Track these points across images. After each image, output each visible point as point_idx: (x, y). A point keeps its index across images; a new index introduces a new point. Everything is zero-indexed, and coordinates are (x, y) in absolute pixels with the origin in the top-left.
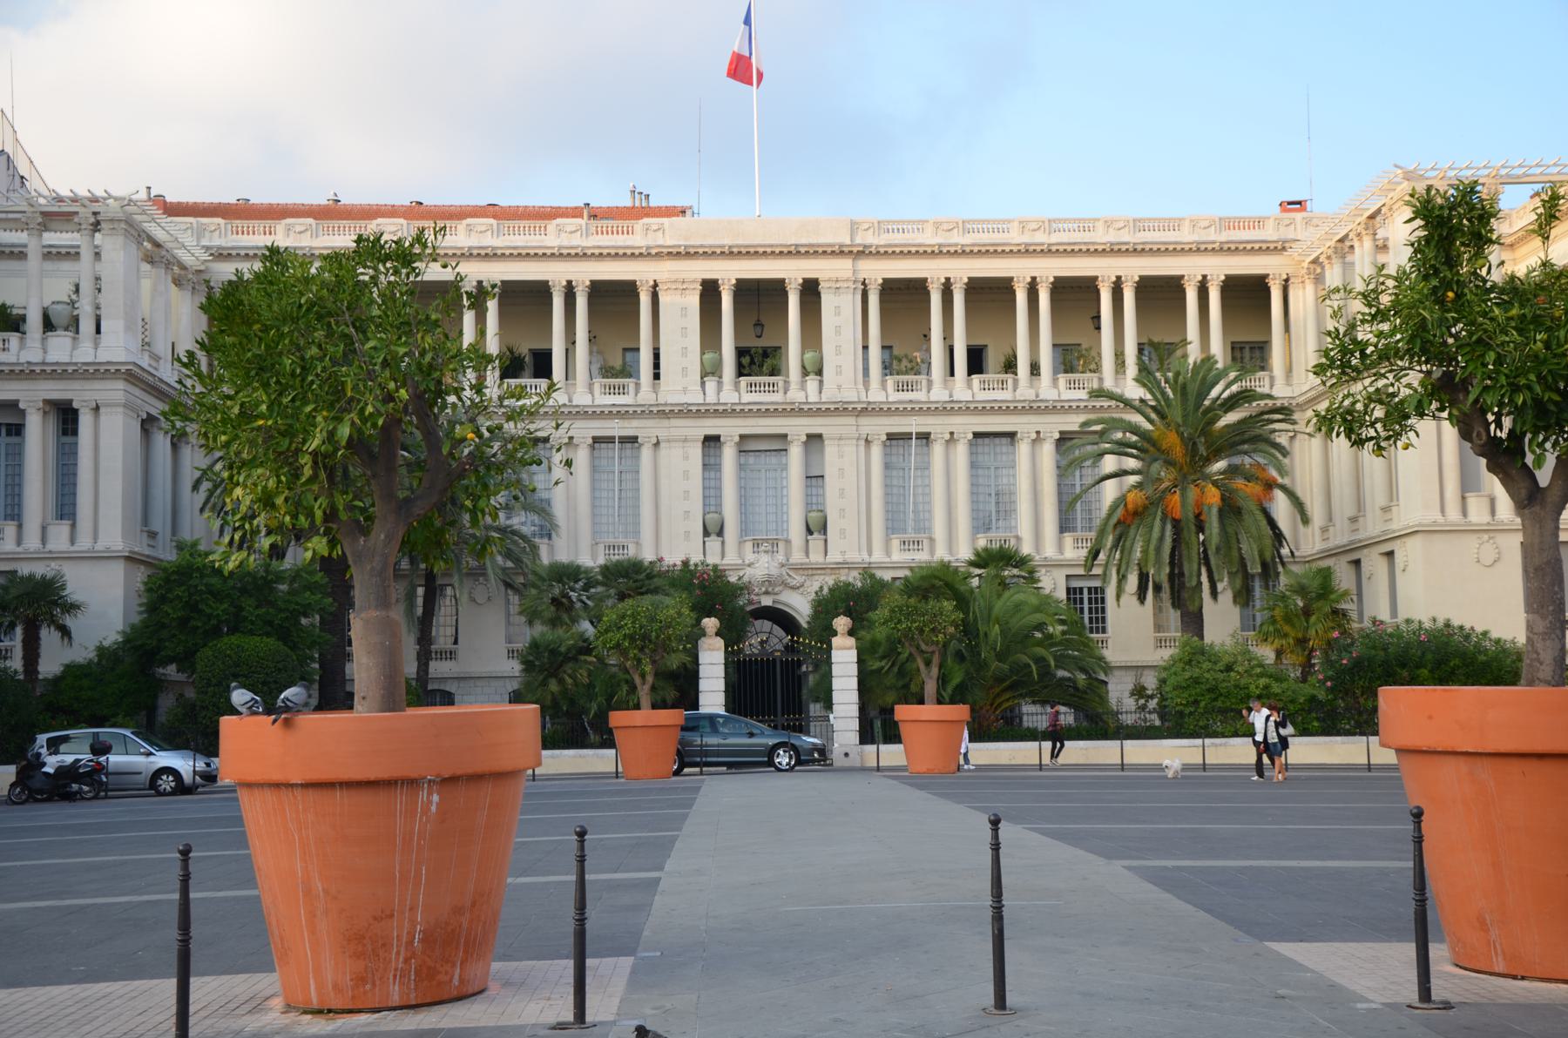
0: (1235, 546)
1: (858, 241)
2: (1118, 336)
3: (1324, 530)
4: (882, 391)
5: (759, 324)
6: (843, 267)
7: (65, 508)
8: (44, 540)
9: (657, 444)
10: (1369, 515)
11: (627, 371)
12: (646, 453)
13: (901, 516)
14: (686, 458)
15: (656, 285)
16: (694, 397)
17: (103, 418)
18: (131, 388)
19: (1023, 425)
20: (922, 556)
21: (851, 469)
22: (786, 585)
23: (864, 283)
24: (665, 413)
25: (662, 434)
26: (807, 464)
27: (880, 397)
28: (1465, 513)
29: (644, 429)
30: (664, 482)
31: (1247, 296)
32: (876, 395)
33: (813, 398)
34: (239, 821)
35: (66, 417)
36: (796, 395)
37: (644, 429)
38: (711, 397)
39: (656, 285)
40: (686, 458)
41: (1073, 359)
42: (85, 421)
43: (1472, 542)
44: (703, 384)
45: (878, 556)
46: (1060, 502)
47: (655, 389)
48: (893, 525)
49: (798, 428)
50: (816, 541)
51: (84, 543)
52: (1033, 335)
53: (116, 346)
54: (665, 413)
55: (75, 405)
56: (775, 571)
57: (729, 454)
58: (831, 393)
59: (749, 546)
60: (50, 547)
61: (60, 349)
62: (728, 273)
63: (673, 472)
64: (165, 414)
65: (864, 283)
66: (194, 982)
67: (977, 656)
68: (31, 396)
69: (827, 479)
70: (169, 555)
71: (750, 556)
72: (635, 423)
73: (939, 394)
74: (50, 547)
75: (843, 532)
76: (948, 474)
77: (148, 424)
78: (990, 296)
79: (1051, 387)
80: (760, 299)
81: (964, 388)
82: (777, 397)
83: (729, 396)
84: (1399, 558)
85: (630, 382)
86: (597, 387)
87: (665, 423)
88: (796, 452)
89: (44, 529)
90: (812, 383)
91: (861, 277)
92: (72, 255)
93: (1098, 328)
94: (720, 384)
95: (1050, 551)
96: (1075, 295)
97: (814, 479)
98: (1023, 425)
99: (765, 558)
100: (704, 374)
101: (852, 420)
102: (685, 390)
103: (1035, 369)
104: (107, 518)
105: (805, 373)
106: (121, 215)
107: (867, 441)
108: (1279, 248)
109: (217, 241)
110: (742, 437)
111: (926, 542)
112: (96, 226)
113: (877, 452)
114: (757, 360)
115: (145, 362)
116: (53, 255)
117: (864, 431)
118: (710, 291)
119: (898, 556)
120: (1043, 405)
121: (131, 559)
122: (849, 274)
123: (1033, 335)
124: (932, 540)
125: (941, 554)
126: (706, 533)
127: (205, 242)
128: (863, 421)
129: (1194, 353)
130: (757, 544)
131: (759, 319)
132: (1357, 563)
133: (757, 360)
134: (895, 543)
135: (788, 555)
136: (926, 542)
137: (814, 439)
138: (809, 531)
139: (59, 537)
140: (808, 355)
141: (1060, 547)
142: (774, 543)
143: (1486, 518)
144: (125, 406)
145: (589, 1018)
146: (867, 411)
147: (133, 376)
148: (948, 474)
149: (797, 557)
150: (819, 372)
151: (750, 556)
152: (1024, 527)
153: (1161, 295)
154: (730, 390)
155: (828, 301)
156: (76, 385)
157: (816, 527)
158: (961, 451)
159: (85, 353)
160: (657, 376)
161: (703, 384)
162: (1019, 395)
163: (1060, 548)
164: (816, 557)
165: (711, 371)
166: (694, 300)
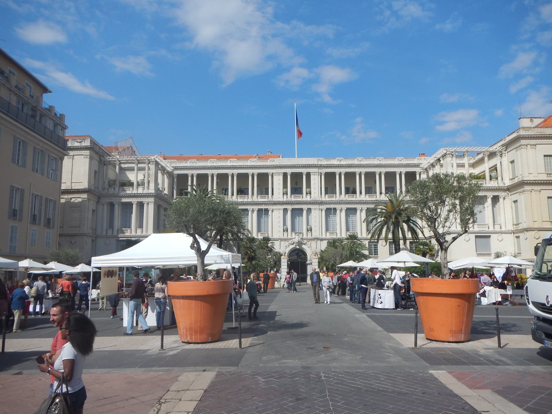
1: (319, 163)
2: (380, 185)
4: (326, 198)
5: (296, 182)
6: (316, 170)
8: (107, 233)
9: (273, 211)
12: (270, 212)
16: (281, 199)
21: (317, 217)
27: (256, 200)
35: (141, 205)
37: (270, 207)
38: (285, 200)
41: (370, 190)
42: (145, 206)
49: (305, 207)
52: (360, 184)
61: (140, 191)
62: (289, 171)
66: (6, 340)
68: (134, 201)
73: (250, 200)
76: (340, 218)
79: (364, 197)
80: (296, 177)
83: (289, 199)
89: (107, 230)
90: (308, 196)
92: (143, 169)
98: (358, 207)
103: (361, 193)
105: (307, 194)
109: (174, 165)
112: (149, 163)
113: (324, 212)
114: (296, 190)
116: (140, 169)
118: (285, 175)
125: (339, 236)
126: (284, 231)
132: (518, 237)
133: (296, 190)
135: (303, 236)
137: (309, 210)
138: (308, 231)
139: (139, 231)
140: (308, 190)
142: (300, 233)
145: (164, 348)
146: (322, 203)
148: (340, 218)
149: (305, 236)
150: (310, 194)
152: (359, 231)
154: (290, 198)
155: (312, 177)
157: (310, 230)
160: (273, 194)
162: (303, 200)
164: (309, 236)
165: (285, 193)
166: (281, 178)
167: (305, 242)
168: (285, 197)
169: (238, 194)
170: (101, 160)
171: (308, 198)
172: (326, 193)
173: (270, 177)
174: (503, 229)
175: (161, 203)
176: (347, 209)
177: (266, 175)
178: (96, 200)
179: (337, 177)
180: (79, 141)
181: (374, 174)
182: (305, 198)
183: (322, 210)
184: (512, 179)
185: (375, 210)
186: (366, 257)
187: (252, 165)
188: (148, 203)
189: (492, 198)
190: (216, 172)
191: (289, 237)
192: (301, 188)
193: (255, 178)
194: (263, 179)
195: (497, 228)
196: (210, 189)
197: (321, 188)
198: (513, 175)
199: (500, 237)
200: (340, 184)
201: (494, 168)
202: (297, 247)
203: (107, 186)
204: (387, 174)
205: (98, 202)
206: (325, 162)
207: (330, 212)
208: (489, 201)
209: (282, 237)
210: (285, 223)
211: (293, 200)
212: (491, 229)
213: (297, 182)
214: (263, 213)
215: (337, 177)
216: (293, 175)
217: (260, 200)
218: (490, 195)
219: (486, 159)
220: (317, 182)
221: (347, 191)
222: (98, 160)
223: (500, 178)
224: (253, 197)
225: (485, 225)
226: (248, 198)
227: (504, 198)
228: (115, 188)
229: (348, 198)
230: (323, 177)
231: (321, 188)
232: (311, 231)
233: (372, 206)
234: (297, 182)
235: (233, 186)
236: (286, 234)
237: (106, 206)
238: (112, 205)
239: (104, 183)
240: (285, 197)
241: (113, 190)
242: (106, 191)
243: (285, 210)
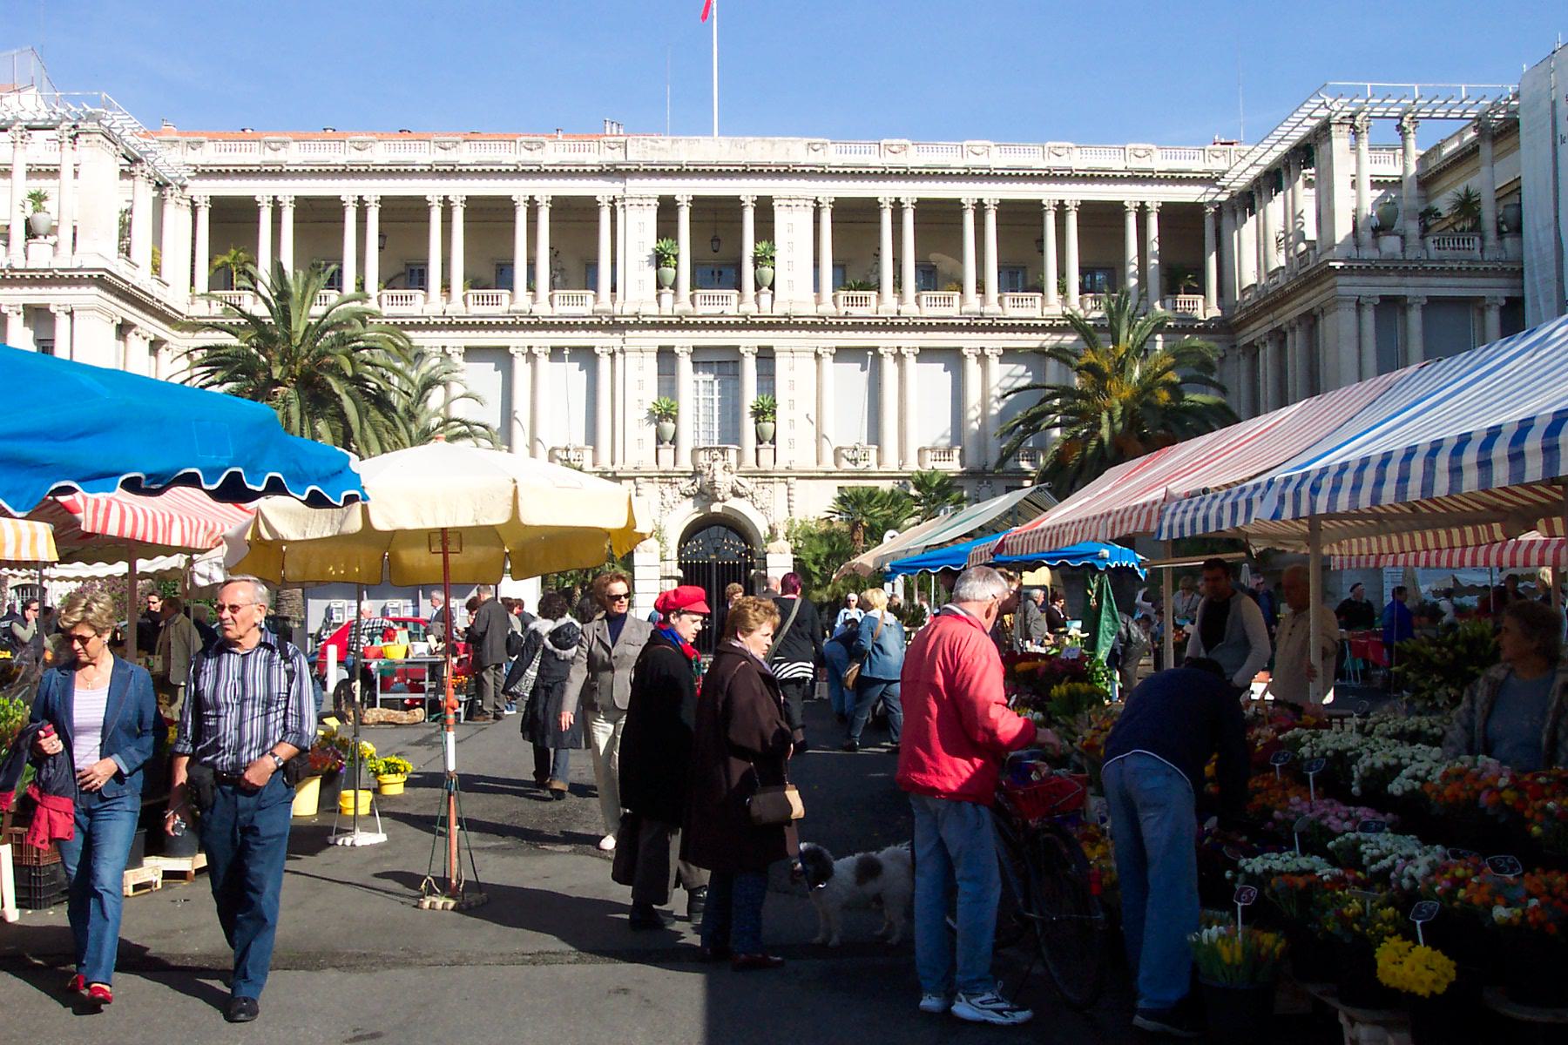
0: (951, 548)
2: (1061, 255)
11: (591, 283)
14: (641, 368)
16: (650, 309)
23: (816, 201)
24: (615, 326)
34: (1283, 402)
40: (641, 368)
44: (659, 296)
47: (613, 299)
49: (748, 342)
52: (980, 252)
54: (615, 326)
55: (53, 309)
57: (685, 364)
61: (41, 256)
62: (684, 190)
65: (816, 201)
79: (462, 302)
80: (717, 219)
85: (419, 294)
113: (1369, 316)
115: (120, 268)
118: (667, 208)
120: (903, 322)
123: (980, 252)
154: (682, 302)
155: (781, 217)
159: (64, 261)
166: (650, 217)
168: (667, 296)
169: (694, 286)
171: (765, 307)
172: (841, 282)
173: (605, 216)
177: (588, 208)
179: (887, 218)
181: (504, 207)
187: (531, 161)
189: (1502, 310)
190: (910, 192)
194: (576, 224)
200: (898, 249)
204: (475, 206)
206: (833, 156)
209: (648, 464)
211: (1012, 312)
213: (718, 240)
215: (887, 218)
217: (477, 310)
220: (795, 234)
221: (930, 278)
229: (935, 306)
234: (718, 240)
235: (362, 252)
236: (667, 454)
240: (667, 296)
243: (666, 355)
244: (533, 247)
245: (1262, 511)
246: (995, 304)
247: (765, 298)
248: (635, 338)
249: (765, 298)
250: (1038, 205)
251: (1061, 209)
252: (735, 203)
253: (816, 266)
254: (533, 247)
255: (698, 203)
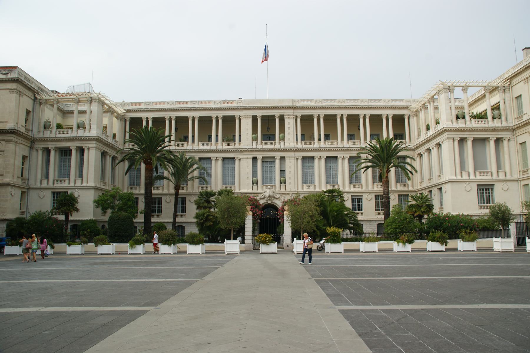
1: (295, 105)
3: (421, 183)
4: (301, 145)
5: (268, 128)
6: (290, 112)
7: (81, 175)
9: (240, 159)
10: (434, 178)
12: (237, 162)
13: (307, 179)
14: (248, 163)
15: (240, 116)
16: (250, 146)
17: (90, 151)
18: (98, 143)
19: (340, 154)
20: (312, 190)
21: (293, 167)
22: (274, 198)
25: (241, 156)
26: (281, 167)
28: (498, 176)
29: (236, 156)
30: (241, 169)
31: (399, 121)
32: (299, 146)
33: (282, 146)
35: (81, 151)
36: (277, 146)
37: (236, 156)
38: (255, 146)
39: (240, 116)
42: (86, 152)
43: (464, 185)
44: (252, 143)
45: (300, 190)
46: (350, 173)
48: (304, 181)
49: (278, 155)
50: (283, 185)
51: (85, 184)
52: (342, 130)
53: (94, 132)
56: (271, 194)
57: (259, 162)
58: (287, 146)
59: (264, 187)
60: (42, 186)
61: (81, 133)
62: (259, 113)
63: (244, 168)
64: (106, 150)
67: (328, 219)
68: (73, 146)
69: (286, 172)
70: (109, 187)
71: (265, 190)
72: (234, 154)
73: (213, 147)
74: (42, 186)
75: (290, 183)
76: (319, 167)
77: (104, 154)
78: (330, 120)
79: (347, 144)
80: (268, 121)
81: (323, 144)
82: (272, 146)
83: (259, 146)
84: (444, 190)
86: (224, 144)
87: (242, 154)
88: (278, 162)
91: (295, 114)
93: (359, 129)
94: (257, 143)
95: (347, 189)
96: (353, 120)
97: (283, 172)
98: (340, 154)
99: (268, 190)
100: (253, 140)
101: (293, 153)
102: (247, 145)
104: (91, 178)
105: (280, 140)
106: (97, 98)
107: (297, 159)
108: (406, 108)
110: (263, 157)
111: (313, 186)
113: (300, 161)
114: (268, 136)
115: (103, 137)
117: (296, 156)
118: (254, 119)
119: (305, 190)
121: (96, 189)
122: (292, 114)
123: (342, 130)
124: (315, 186)
125: (318, 190)
126: (253, 183)
127: (124, 108)
128: (296, 153)
129: (385, 136)
130: (267, 186)
131: (268, 125)
133: (268, 136)
134: (305, 186)
135: (275, 189)
136: (313, 186)
137: (283, 158)
138: (281, 183)
140: (281, 135)
141: (350, 188)
143: (467, 178)
144: (96, 148)
147: (97, 139)
148: (319, 167)
149: (278, 190)
151: (265, 190)
152: (340, 182)
153: (376, 120)
154: (259, 145)
155: (286, 121)
156: (84, 142)
157: (283, 182)
158: (323, 161)
159: (87, 134)
160: (240, 141)
161: (252, 143)
163: (396, 187)
164: (283, 190)
165: (255, 139)
166: (250, 121)
167: (278, 196)
168: (255, 143)
170: (36, 98)
172: (303, 138)
174: (508, 177)
175: (107, 149)
176: (328, 158)
178: (29, 145)
180: (4, 72)
182: (277, 144)
183: (297, 159)
184: (518, 118)
185: (358, 157)
186: (349, 163)
188: (89, 149)
191: (260, 190)
192: (274, 135)
193: (220, 122)
194: (229, 123)
195: (502, 176)
196: (167, 134)
197: (297, 135)
198: (519, 113)
199: (505, 186)
200: (319, 129)
201: (496, 108)
202: (269, 202)
203: (42, 129)
204: (372, 117)
205: (31, 147)
207: (308, 160)
208: (492, 143)
210: (254, 174)
212: (495, 177)
214: (228, 161)
216: (264, 117)
218: (493, 136)
219: (487, 95)
221: (351, 137)
222: (33, 98)
223: (503, 118)
224: (217, 144)
225: (488, 172)
226: (211, 145)
227: (509, 140)
228: (51, 131)
230: (299, 121)
231: (297, 135)
232: (285, 183)
233: (354, 154)
236: (255, 186)
237: (40, 152)
238: (47, 151)
239: (39, 125)
240: (255, 143)
241: (49, 132)
242: (41, 134)
243: (255, 159)
244: (217, 130)
245: (47, 214)
246: (347, 144)
247: (282, 143)
248: (246, 155)
249: (282, 143)
250: (335, 116)
251: (365, 117)
252: (273, 117)
253: (240, 135)
254: (217, 130)
255: (263, 116)
